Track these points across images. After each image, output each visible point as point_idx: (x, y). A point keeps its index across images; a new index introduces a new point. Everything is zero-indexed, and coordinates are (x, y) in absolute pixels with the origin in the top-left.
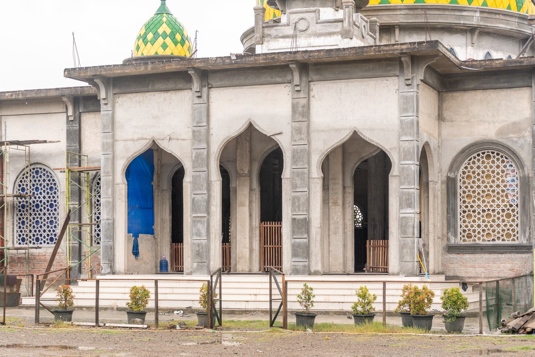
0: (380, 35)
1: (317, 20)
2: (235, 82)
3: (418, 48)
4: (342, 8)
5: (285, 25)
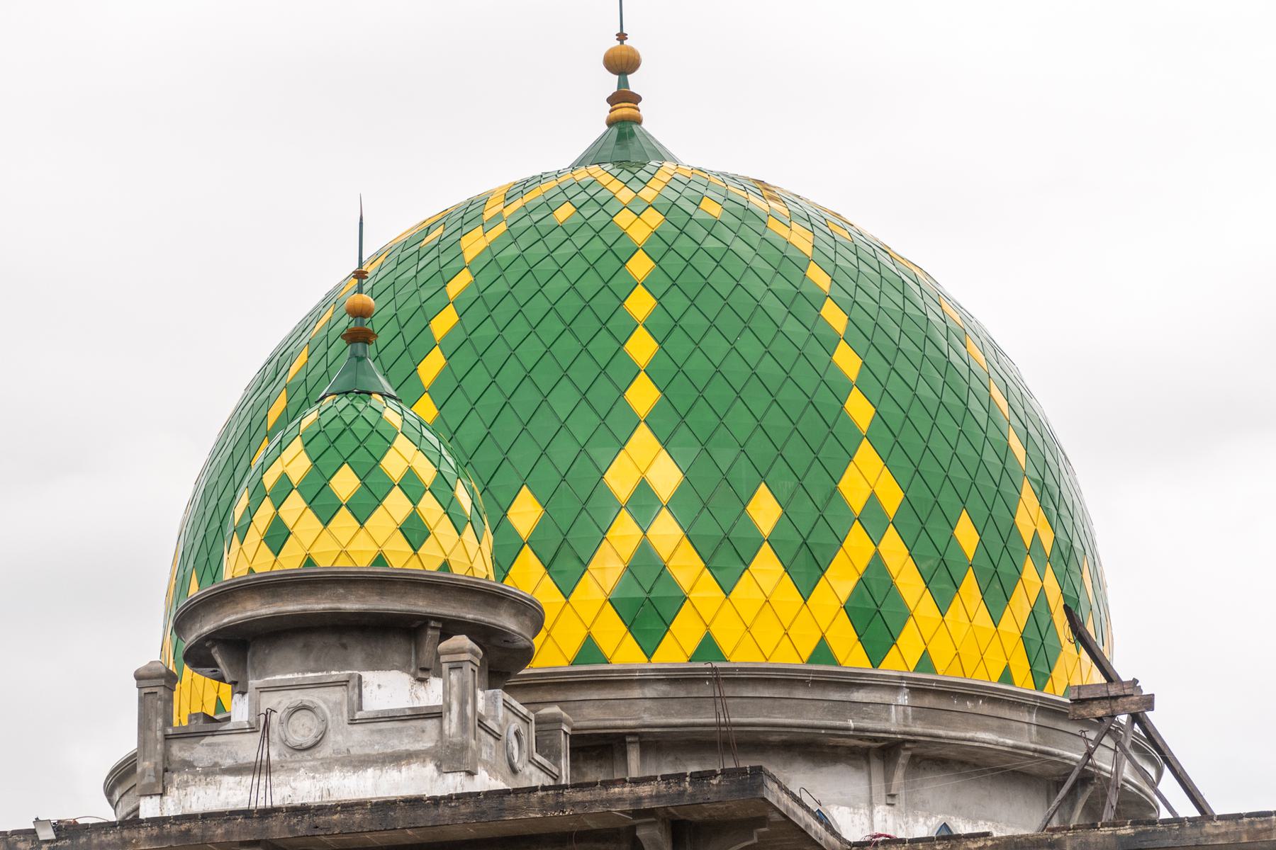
0: (573, 760)
1: (351, 712)
3: (692, 795)
4: (438, 674)
5: (241, 731)
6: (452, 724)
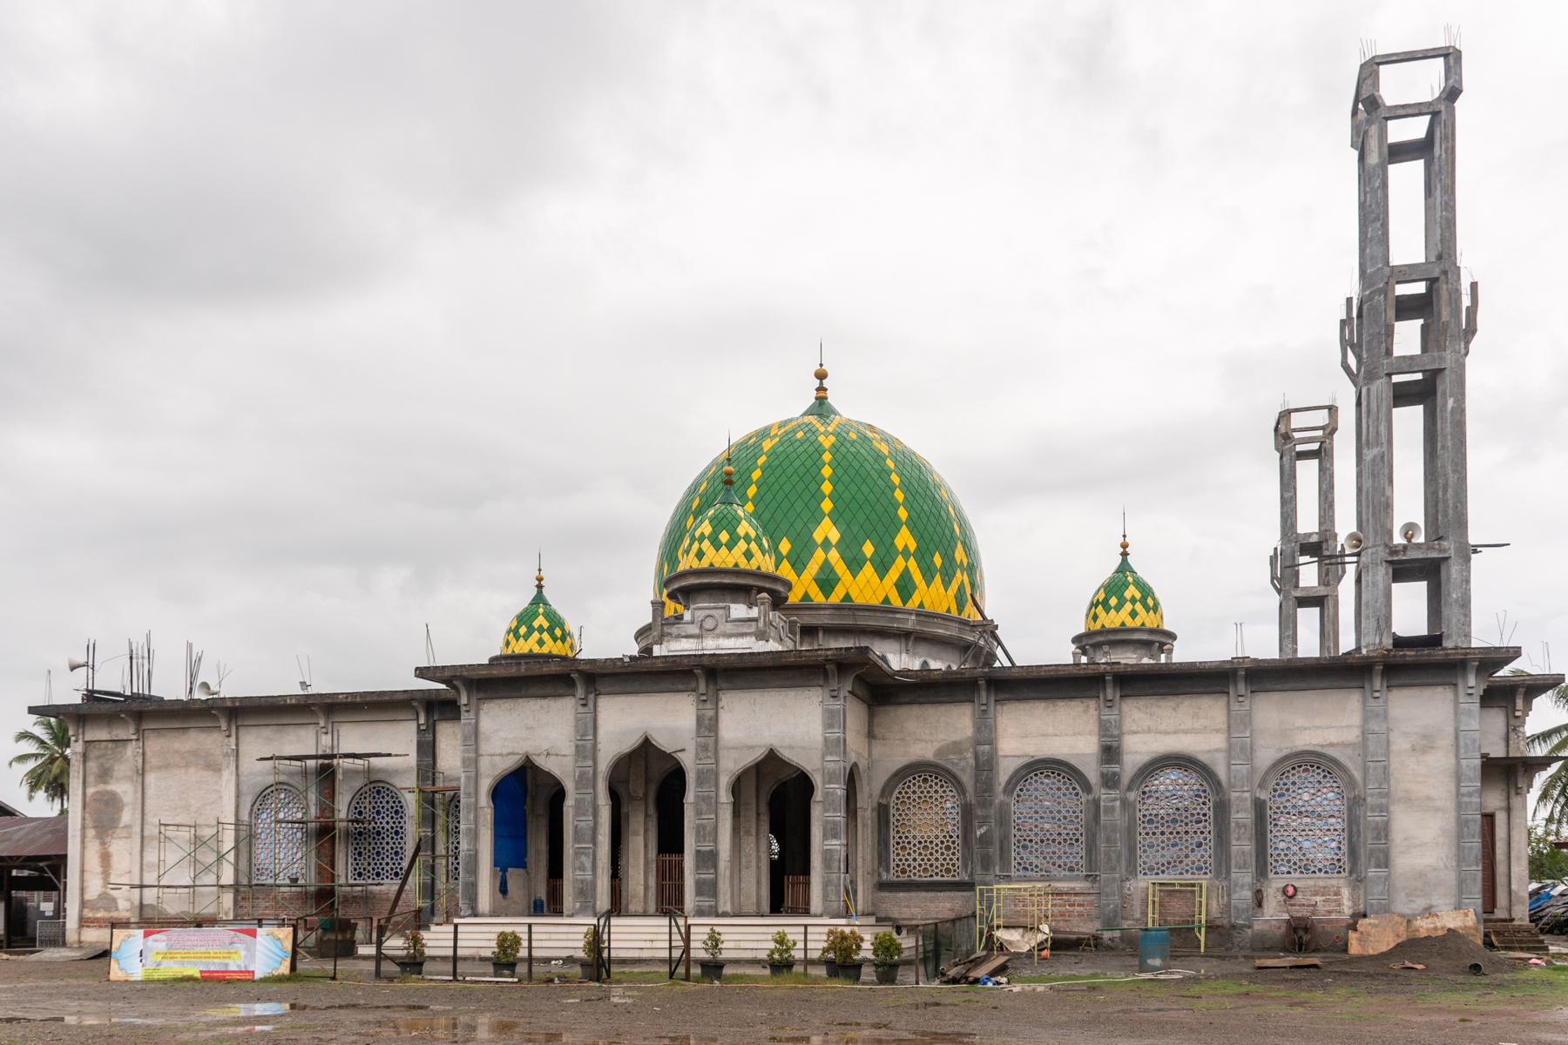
6: (761, 624)
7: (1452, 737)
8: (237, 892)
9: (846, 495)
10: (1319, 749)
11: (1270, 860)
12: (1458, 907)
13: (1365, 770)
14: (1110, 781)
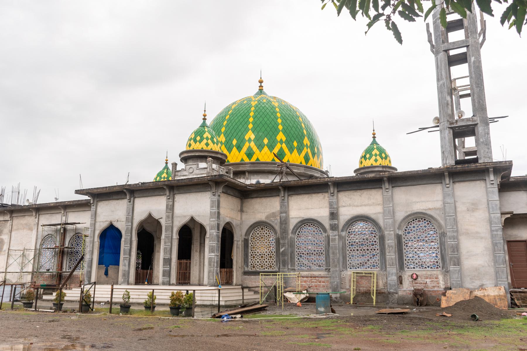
2: (145, 195)
6: (208, 169)
7: (486, 204)
8: (33, 274)
9: (258, 122)
10: (424, 211)
11: (405, 262)
12: (496, 286)
13: (446, 220)
14: (334, 227)
